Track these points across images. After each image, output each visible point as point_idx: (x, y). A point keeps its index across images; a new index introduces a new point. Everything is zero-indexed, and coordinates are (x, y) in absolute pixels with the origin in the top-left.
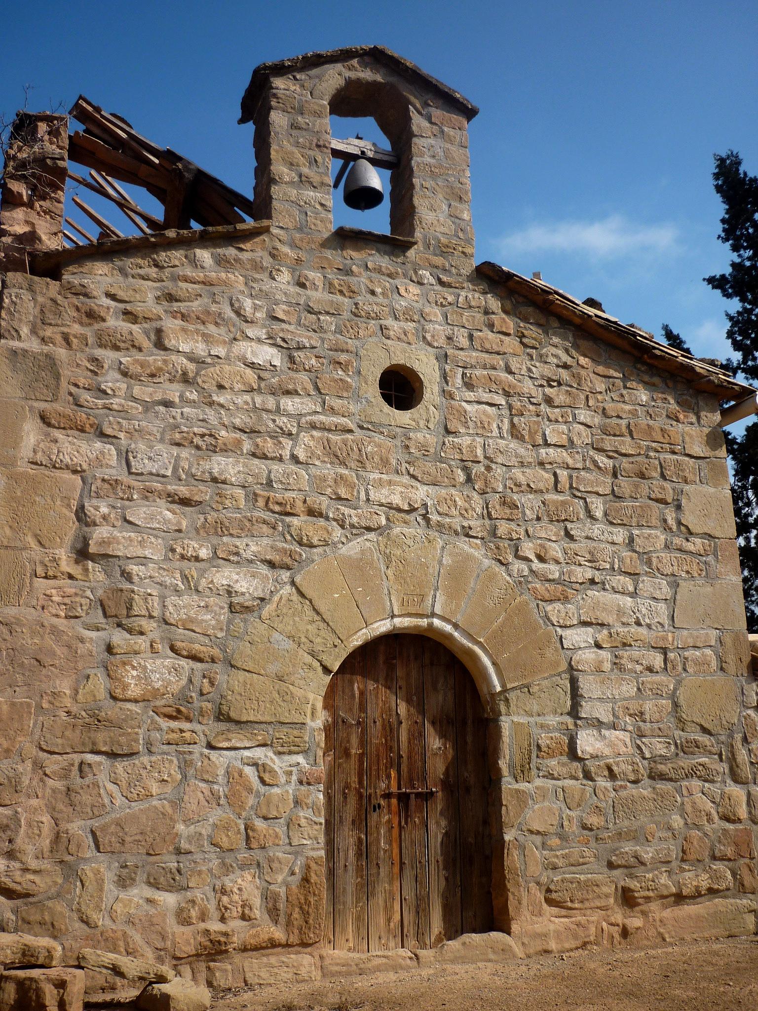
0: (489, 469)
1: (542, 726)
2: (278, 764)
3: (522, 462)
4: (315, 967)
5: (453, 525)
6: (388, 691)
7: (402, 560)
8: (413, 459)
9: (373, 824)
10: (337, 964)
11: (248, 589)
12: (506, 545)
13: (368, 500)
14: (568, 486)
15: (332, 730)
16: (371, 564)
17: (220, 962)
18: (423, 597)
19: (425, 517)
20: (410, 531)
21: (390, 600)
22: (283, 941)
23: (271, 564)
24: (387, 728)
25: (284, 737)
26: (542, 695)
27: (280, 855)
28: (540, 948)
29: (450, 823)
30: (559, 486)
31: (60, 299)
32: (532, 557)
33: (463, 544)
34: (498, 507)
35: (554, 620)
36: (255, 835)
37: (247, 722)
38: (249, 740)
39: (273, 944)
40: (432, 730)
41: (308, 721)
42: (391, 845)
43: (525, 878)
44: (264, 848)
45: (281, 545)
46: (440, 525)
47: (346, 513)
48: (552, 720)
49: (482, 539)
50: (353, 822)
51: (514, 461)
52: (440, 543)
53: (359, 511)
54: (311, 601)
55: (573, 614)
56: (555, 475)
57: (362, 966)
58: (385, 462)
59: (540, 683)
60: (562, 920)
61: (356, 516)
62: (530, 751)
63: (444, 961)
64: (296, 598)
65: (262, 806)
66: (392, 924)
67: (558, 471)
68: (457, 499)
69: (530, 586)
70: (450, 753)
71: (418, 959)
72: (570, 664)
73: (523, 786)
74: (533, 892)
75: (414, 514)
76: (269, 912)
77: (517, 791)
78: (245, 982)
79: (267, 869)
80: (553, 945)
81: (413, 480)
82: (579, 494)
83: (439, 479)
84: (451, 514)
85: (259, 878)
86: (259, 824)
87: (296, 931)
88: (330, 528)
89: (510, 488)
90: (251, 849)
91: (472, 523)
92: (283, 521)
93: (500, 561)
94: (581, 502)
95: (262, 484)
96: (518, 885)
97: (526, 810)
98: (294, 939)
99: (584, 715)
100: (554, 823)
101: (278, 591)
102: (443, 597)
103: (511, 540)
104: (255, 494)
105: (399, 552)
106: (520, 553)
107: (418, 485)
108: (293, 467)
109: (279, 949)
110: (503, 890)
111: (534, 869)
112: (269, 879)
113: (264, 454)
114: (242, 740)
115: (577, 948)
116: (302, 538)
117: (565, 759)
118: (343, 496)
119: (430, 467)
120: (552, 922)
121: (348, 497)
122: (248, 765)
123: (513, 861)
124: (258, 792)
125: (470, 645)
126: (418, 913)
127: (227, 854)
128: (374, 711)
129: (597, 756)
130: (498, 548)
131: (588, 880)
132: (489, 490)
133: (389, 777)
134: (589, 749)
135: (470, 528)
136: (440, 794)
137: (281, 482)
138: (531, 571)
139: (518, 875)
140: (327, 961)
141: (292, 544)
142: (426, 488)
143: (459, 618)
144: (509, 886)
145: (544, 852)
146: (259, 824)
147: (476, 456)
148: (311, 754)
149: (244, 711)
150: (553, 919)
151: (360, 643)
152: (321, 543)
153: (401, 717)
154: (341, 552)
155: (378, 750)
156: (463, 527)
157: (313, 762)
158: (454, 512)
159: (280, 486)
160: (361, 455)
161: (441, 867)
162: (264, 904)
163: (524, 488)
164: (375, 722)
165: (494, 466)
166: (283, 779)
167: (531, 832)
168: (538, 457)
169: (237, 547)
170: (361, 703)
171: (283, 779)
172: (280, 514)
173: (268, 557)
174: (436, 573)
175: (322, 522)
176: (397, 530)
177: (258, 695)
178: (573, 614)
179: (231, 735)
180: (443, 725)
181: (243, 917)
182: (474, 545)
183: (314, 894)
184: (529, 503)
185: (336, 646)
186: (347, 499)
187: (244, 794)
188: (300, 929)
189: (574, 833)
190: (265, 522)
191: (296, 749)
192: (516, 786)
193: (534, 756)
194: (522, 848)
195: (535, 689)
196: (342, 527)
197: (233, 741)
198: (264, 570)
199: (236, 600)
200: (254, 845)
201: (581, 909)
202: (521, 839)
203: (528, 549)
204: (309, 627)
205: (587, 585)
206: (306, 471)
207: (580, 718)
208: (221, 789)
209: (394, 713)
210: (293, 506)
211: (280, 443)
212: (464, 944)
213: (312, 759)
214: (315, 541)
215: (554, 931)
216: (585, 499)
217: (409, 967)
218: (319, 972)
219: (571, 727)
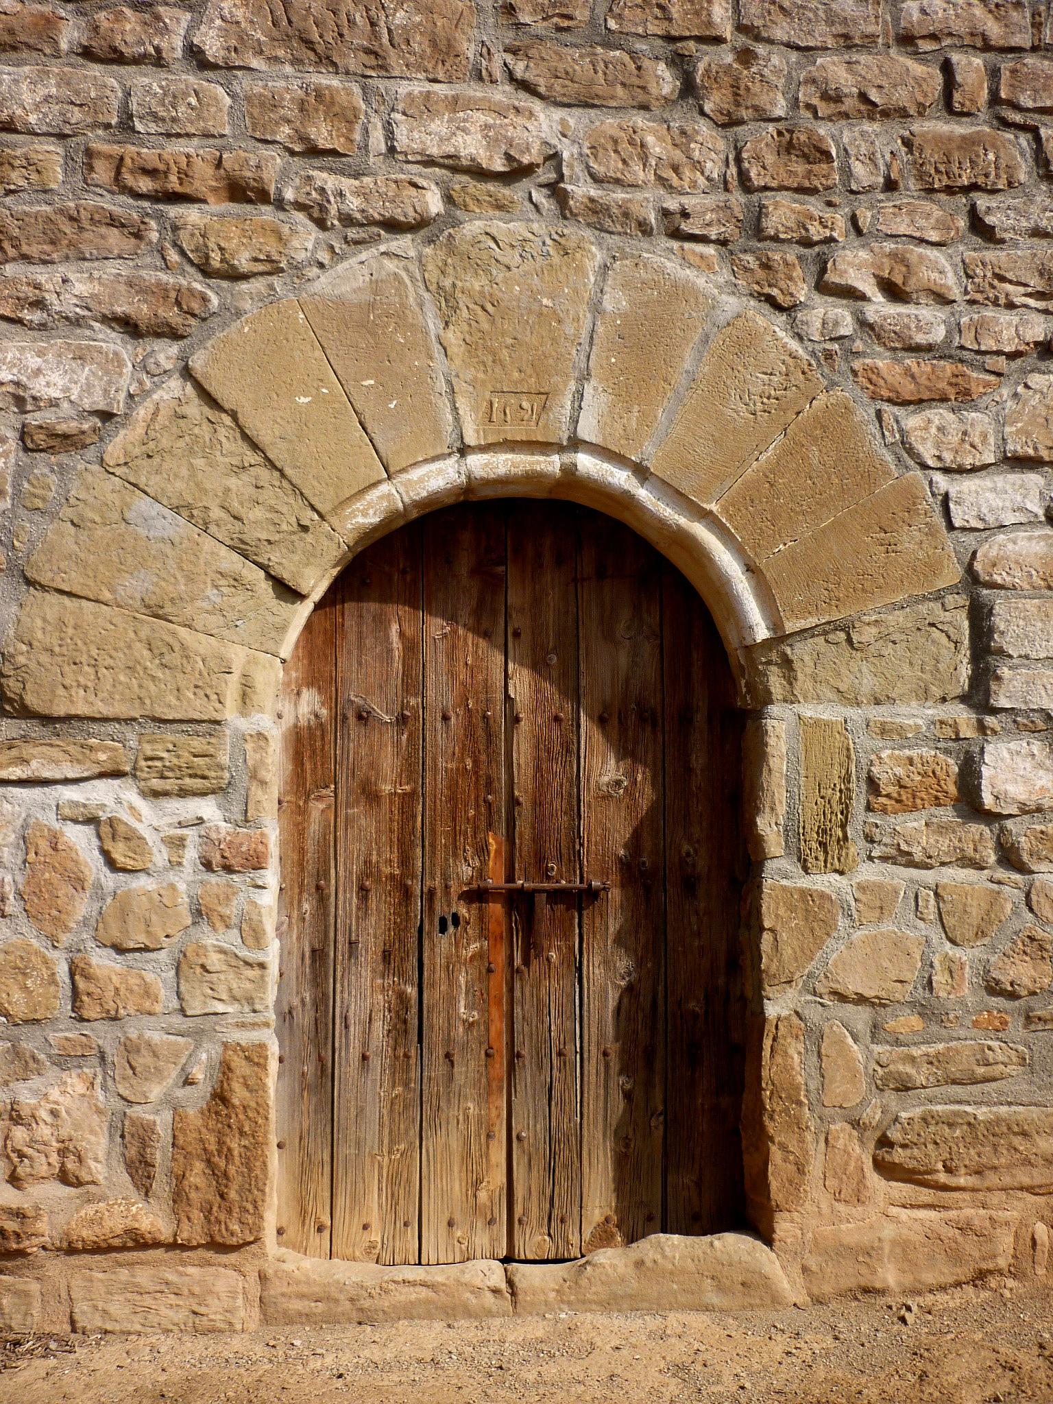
0: (745, 57)
1: (884, 731)
2: (149, 819)
3: (846, 37)
4: (246, 1298)
5: (634, 209)
6: (483, 643)
7: (488, 305)
8: (527, 42)
9: (440, 961)
10: (302, 1296)
11: (66, 390)
12: (791, 258)
13: (392, 150)
14: (985, 95)
15: (330, 737)
16: (400, 316)
17: (12, 1273)
18: (545, 396)
20: (512, 228)
22: (166, 1234)
23: (130, 327)
24: (480, 732)
25: (180, 758)
26: (888, 650)
27: (156, 1037)
28: (851, 1282)
29: (640, 963)
30: (957, 96)
32: (867, 286)
33: (664, 258)
34: (770, 159)
35: (928, 453)
36: (92, 988)
37: (68, 718)
38: (74, 760)
39: (139, 1242)
40: (597, 736)
41: (230, 714)
42: (485, 1011)
43: (818, 1109)
44: (115, 1019)
45: (152, 276)
46: (596, 209)
47: (329, 187)
48: (915, 715)
49: (723, 243)
50: (386, 956)
51: (822, 34)
52: (598, 256)
53: (367, 180)
54: (234, 415)
55: (984, 436)
56: (947, 68)
57: (366, 1304)
58: (444, 51)
59: (880, 617)
60: (922, 1214)
61: (357, 193)
62: (846, 795)
63: (584, 1302)
64: (195, 409)
65: (110, 920)
66: (483, 1196)
67: (955, 57)
68: (650, 139)
69: (857, 364)
70: (646, 797)
71: (513, 1294)
72: (970, 569)
73: (823, 882)
74: (840, 1144)
75: (525, 184)
76: (130, 1166)
77: (805, 894)
78: (73, 1322)
79: (122, 1069)
80: (889, 1276)
81: (522, 95)
82: (1018, 118)
83: (598, 90)
84: (629, 178)
85: (104, 1087)
86: (102, 961)
87: (197, 1216)
88: (285, 229)
89: (808, 106)
90: (82, 1019)
91: (689, 202)
92: (160, 217)
93: (771, 301)
94: (1024, 140)
95: (108, 126)
96: (798, 1125)
97: (830, 942)
98: (193, 1231)
99: (1003, 702)
100: (907, 976)
101: (146, 394)
102: (604, 398)
103: (807, 243)
104: (89, 153)
105: (477, 284)
106: (831, 277)
107: (537, 106)
108: (191, 79)
109: (159, 1253)
110: (762, 1139)
111: (847, 1089)
112: (126, 1093)
113: (115, 50)
114: (57, 762)
115: (958, 1284)
116: (207, 257)
117: (947, 814)
118: (323, 144)
119: (576, 60)
120: (892, 1218)
121: (338, 144)
122: (75, 821)
123: (787, 1069)
124: (98, 886)
125: (683, 521)
126: (551, 1171)
127: (25, 1029)
128: (439, 691)
129: (1039, 809)
130: (766, 266)
131: (998, 1120)
132: (745, 114)
133: (482, 850)
134: (1018, 792)
135: (685, 215)
136: (615, 895)
137: (156, 118)
138: (863, 324)
139: (800, 1103)
140: (276, 1288)
141: (183, 273)
142: (558, 114)
143: (648, 452)
144: (771, 1127)
145: (878, 1049)
146: (102, 961)
147: (710, 24)
148: (236, 796)
149: (61, 691)
150: (894, 1211)
151: (373, 519)
152: (260, 267)
153: (519, 705)
154: (317, 287)
155: (453, 785)
156: (666, 213)
157: (240, 817)
158: (638, 173)
159: (153, 128)
160: (375, 35)
161: (615, 1065)
162: (118, 1149)
163: (850, 104)
164: (445, 718)
165: (761, 49)
166: (160, 856)
167: (842, 998)
168: (896, 20)
169: (38, 287)
170: (406, 673)
171: (160, 856)
172: (155, 198)
173: (119, 310)
175: (267, 213)
176: (472, 228)
177: (94, 652)
178: (984, 436)
179: (27, 750)
180: (628, 726)
181: (64, 1177)
182: (692, 259)
183: (242, 1133)
184: (865, 147)
185: (305, 529)
186: (333, 153)
187: (65, 890)
188: (208, 1211)
189: (962, 1002)
190: (113, 221)
191: (197, 783)
192: (804, 882)
193: (858, 804)
194: (815, 1037)
195: (865, 635)
196: (321, 224)
197: (34, 764)
198: (112, 341)
199: (34, 419)
200: (91, 1011)
201: (974, 1190)
202: (813, 1014)
203: (855, 266)
204: (233, 482)
205: (1032, 360)
206: (227, 86)
207: (995, 711)
208: (8, 879)
209: (500, 696)
210: (184, 175)
211: (158, 18)
212: (640, 1264)
213: (236, 812)
214: (243, 262)
215: (894, 1243)
216: (1034, 131)
217: (490, 1314)
218: (256, 1313)
219: (967, 732)
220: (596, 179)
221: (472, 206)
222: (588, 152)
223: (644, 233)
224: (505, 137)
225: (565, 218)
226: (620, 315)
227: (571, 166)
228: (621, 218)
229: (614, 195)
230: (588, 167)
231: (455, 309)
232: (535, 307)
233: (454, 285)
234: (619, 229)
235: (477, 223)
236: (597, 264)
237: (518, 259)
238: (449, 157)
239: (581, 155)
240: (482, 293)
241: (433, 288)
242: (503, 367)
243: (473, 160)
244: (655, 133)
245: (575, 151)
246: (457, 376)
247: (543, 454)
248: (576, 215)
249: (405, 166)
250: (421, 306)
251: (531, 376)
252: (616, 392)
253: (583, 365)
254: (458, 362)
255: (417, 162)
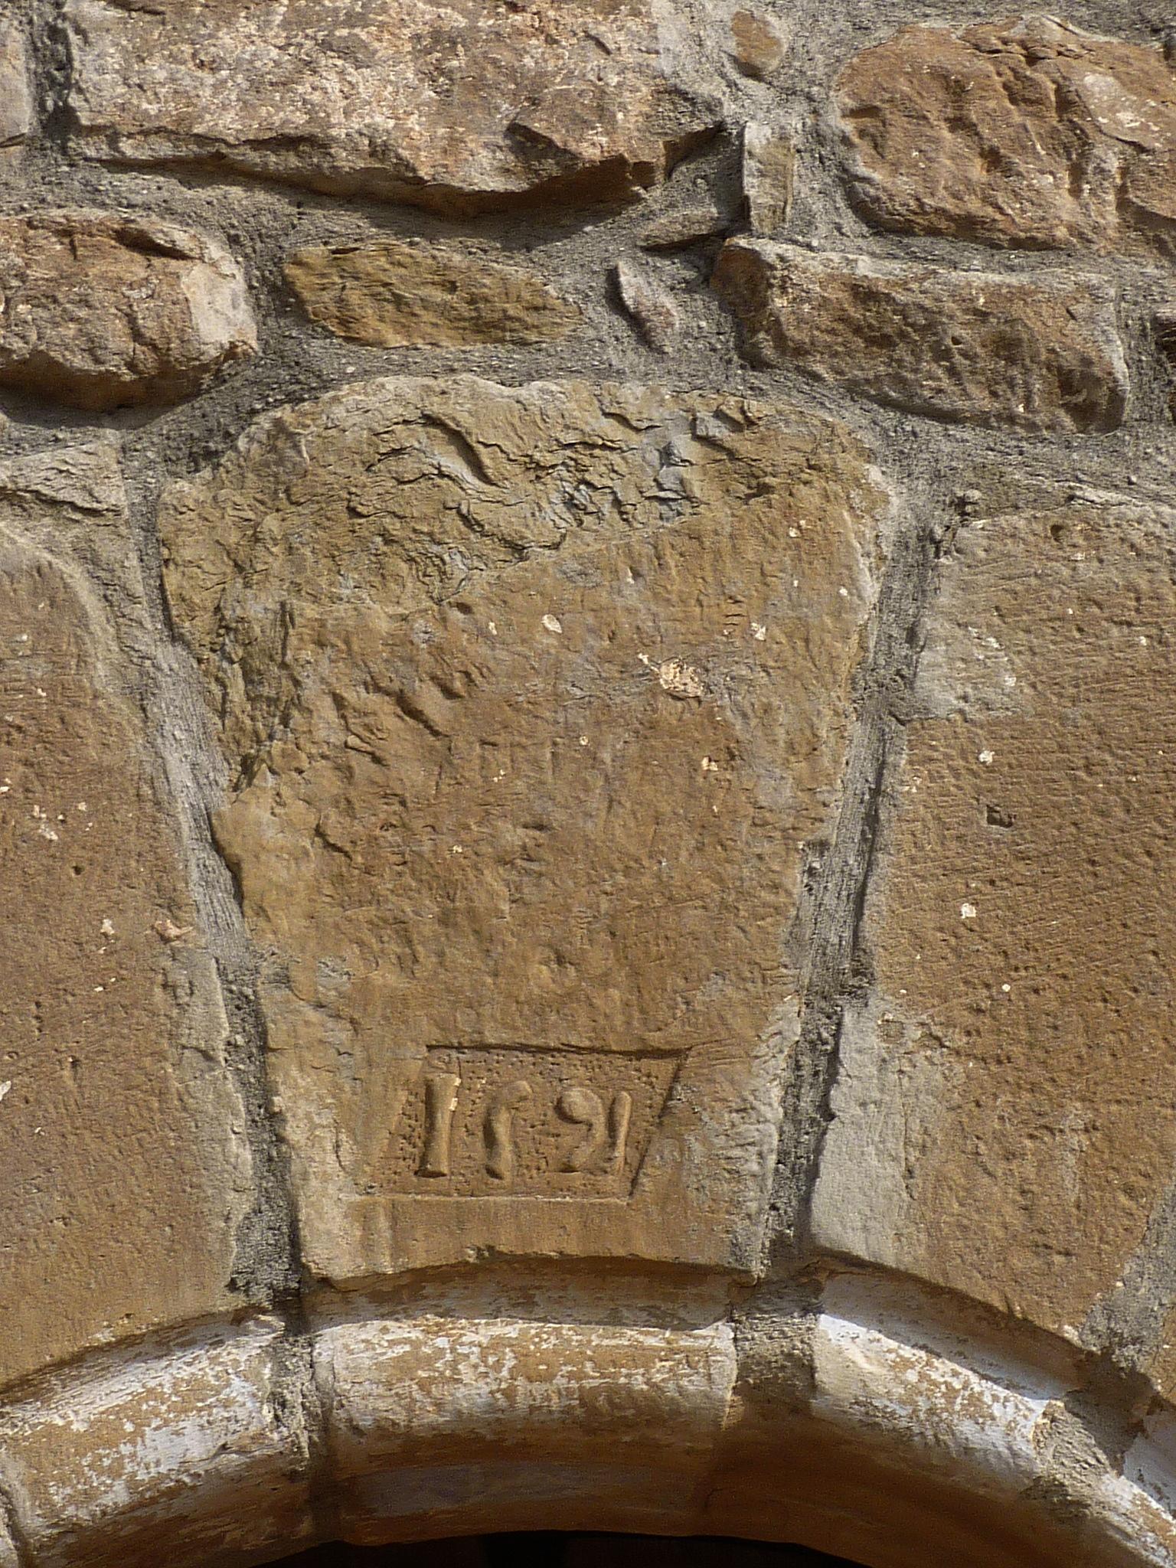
5: (1043, 326)
18: (669, 1067)
19: (721, 266)
21: (268, 1120)
31: (695, 510)
46: (875, 325)
52: (898, 501)
68: (1096, 84)
75: (595, 242)
84: (1019, 216)
102: (930, 1071)
158: (1051, 196)
174: (839, 817)
176: (371, 400)
220: (880, 221)
221: (372, 320)
222: (848, 127)
223: (1084, 414)
224: (512, 74)
225: (754, 362)
226: (993, 728)
227: (777, 174)
228: (987, 364)
229: (955, 276)
230: (847, 181)
231: (286, 708)
232: (628, 698)
233: (285, 617)
234: (982, 400)
235: (391, 383)
236: (887, 530)
237: (555, 514)
238: (287, 142)
239: (818, 137)
240: (400, 644)
241: (199, 627)
242: (485, 939)
243: (380, 150)
244: (1114, 66)
245: (795, 121)
246: (284, 979)
247: (660, 1320)
248: (800, 351)
249: (107, 180)
250: (141, 696)
251: (604, 981)
252: (986, 1043)
253: (836, 933)
254: (288, 921)
255: (157, 166)
